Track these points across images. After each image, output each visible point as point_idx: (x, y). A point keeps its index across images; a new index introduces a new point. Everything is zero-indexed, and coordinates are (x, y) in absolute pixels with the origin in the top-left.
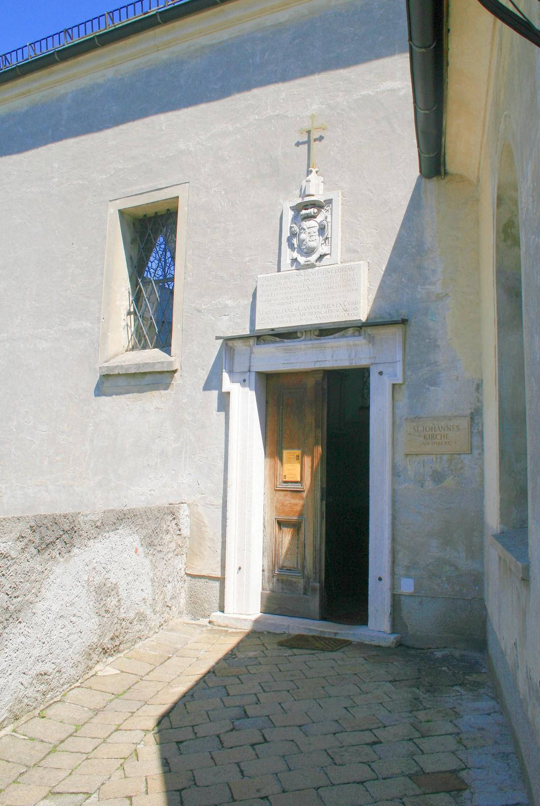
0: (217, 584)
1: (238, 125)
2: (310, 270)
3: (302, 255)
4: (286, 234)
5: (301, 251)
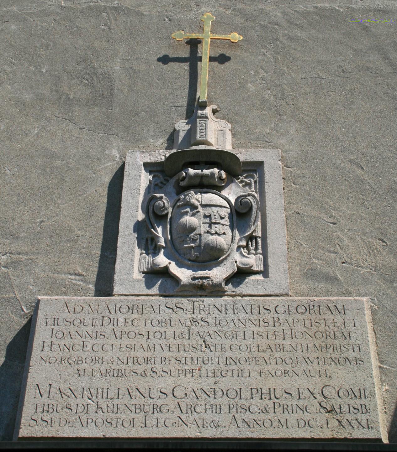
0: (186, 67)
1: (15, 8)
2: (209, 301)
3: (180, 265)
4: (132, 211)
5: (176, 252)
